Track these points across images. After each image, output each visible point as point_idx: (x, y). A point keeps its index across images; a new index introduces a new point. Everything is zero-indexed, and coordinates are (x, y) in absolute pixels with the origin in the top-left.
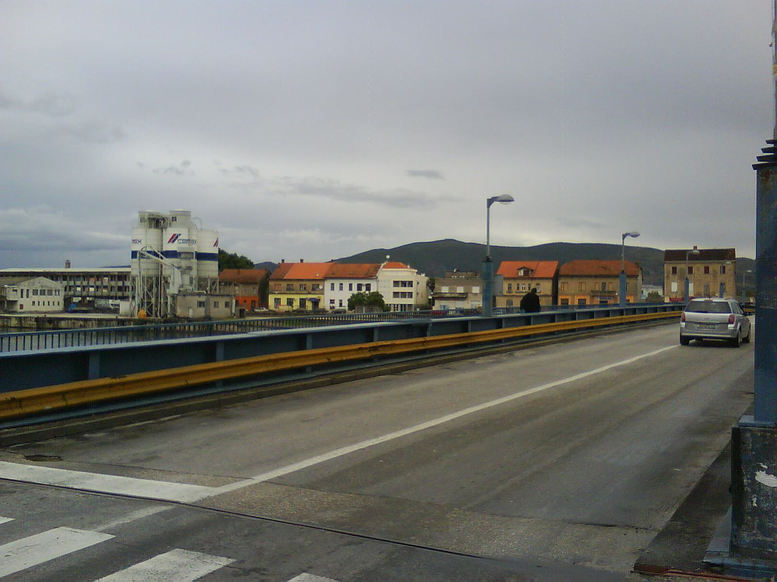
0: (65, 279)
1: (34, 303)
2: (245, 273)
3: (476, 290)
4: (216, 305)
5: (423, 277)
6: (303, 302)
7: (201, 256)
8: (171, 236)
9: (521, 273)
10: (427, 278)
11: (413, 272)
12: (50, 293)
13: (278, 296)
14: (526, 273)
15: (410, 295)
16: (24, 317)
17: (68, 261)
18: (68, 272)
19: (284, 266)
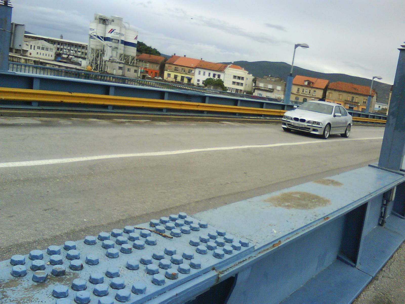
0: (59, 44)
1: (38, 53)
2: (154, 57)
3: (279, 88)
4: (129, 70)
5: (250, 76)
6: (182, 78)
7: (126, 43)
8: (111, 29)
9: (306, 83)
10: (253, 77)
11: (246, 73)
12: (47, 49)
13: (170, 73)
14: (309, 83)
15: (242, 84)
16: (28, 59)
17: (61, 35)
18: (60, 41)
19: (174, 57)
